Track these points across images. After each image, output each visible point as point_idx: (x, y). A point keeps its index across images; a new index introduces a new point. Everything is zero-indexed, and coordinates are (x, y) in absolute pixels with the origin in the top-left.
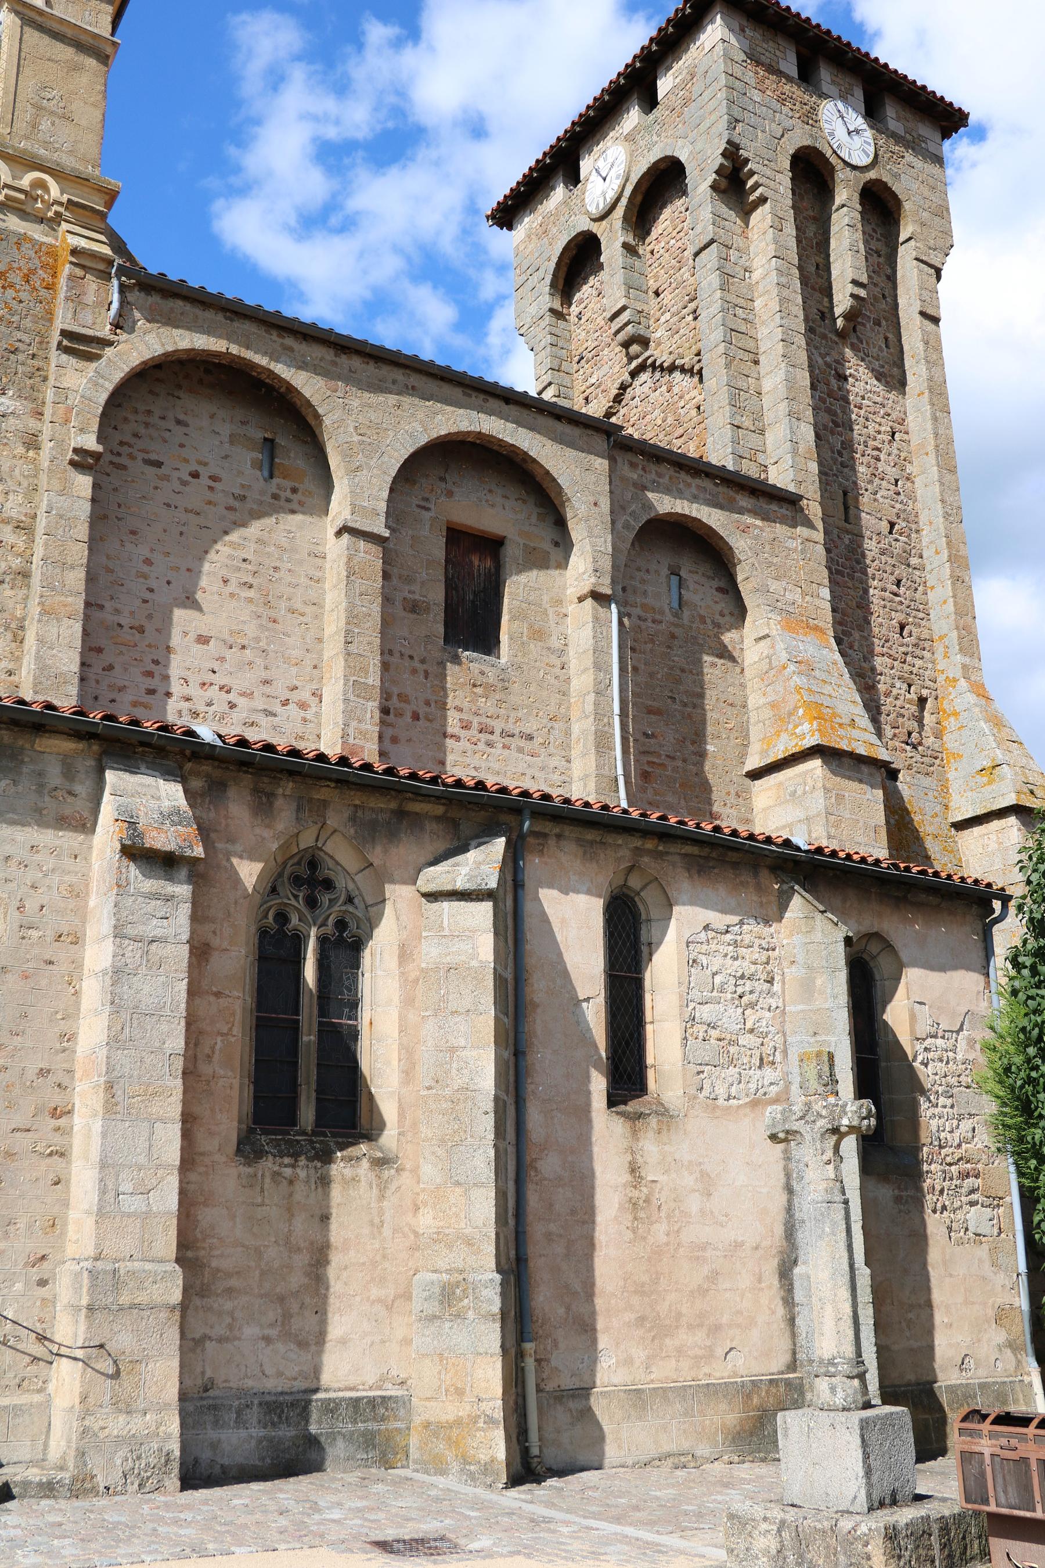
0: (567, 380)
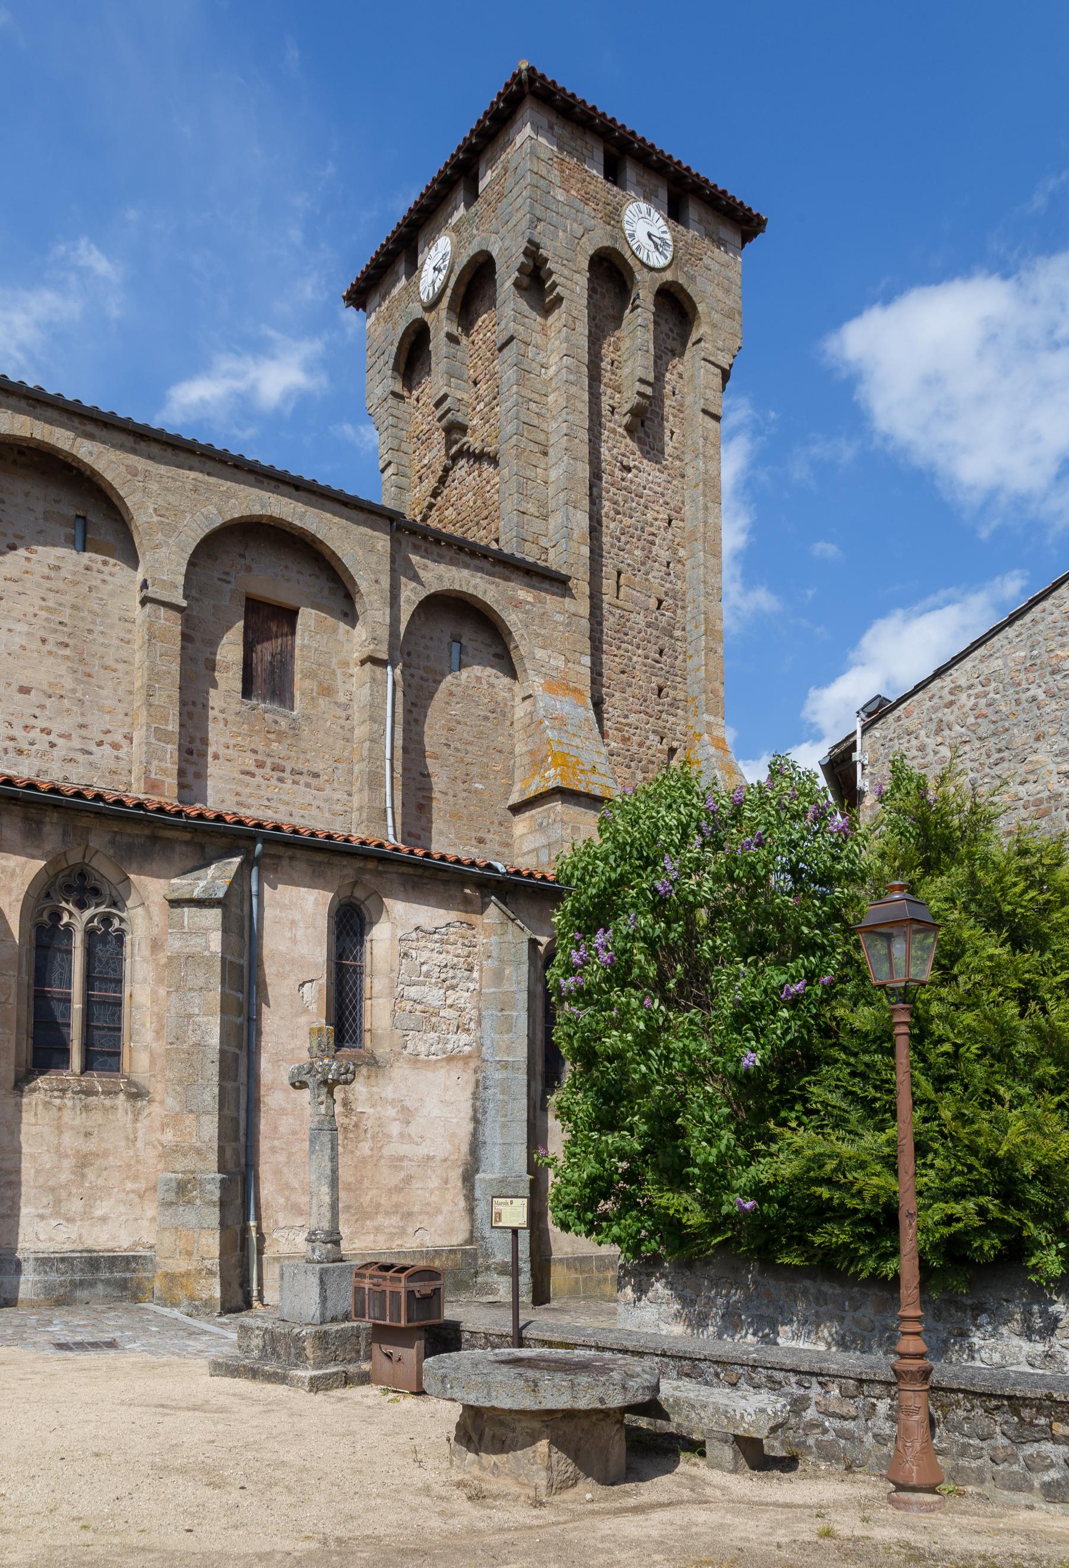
0: (405, 460)
